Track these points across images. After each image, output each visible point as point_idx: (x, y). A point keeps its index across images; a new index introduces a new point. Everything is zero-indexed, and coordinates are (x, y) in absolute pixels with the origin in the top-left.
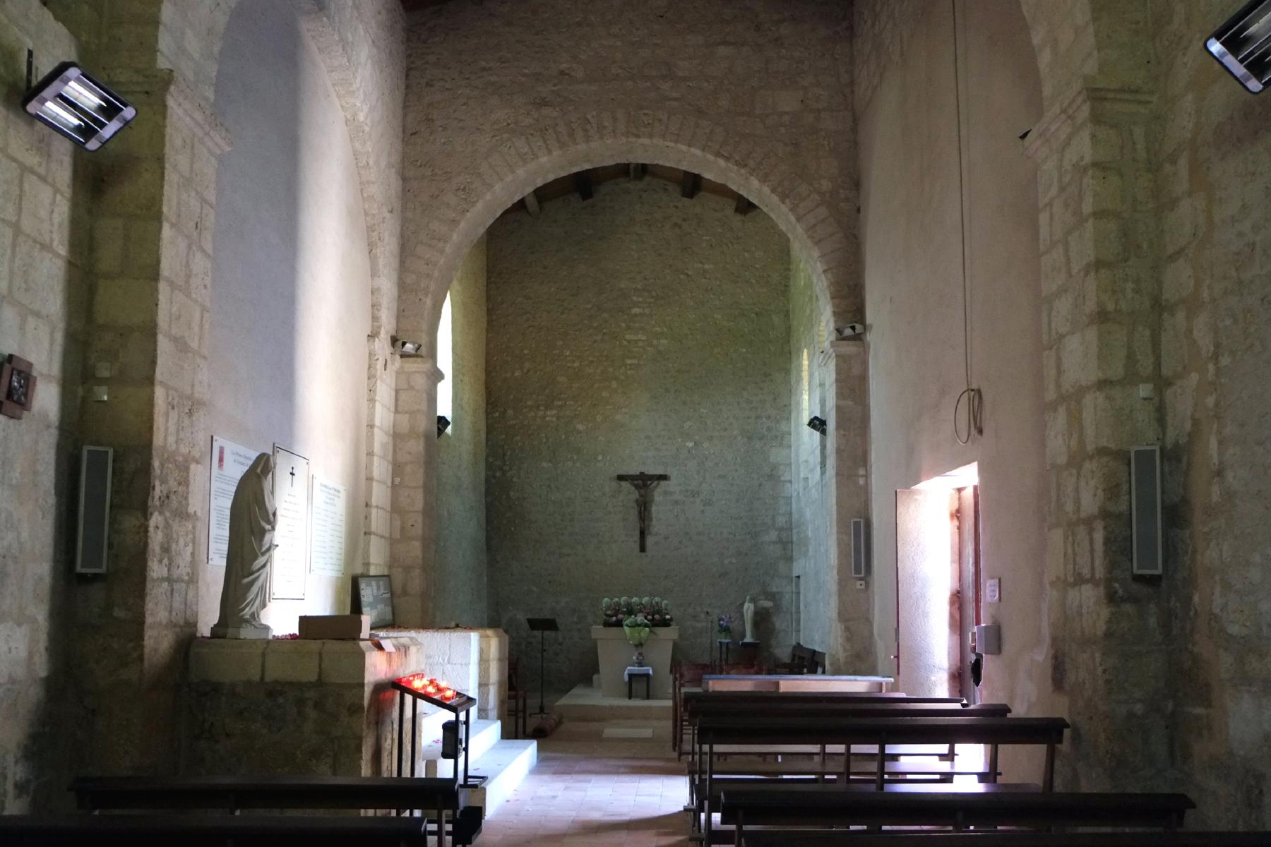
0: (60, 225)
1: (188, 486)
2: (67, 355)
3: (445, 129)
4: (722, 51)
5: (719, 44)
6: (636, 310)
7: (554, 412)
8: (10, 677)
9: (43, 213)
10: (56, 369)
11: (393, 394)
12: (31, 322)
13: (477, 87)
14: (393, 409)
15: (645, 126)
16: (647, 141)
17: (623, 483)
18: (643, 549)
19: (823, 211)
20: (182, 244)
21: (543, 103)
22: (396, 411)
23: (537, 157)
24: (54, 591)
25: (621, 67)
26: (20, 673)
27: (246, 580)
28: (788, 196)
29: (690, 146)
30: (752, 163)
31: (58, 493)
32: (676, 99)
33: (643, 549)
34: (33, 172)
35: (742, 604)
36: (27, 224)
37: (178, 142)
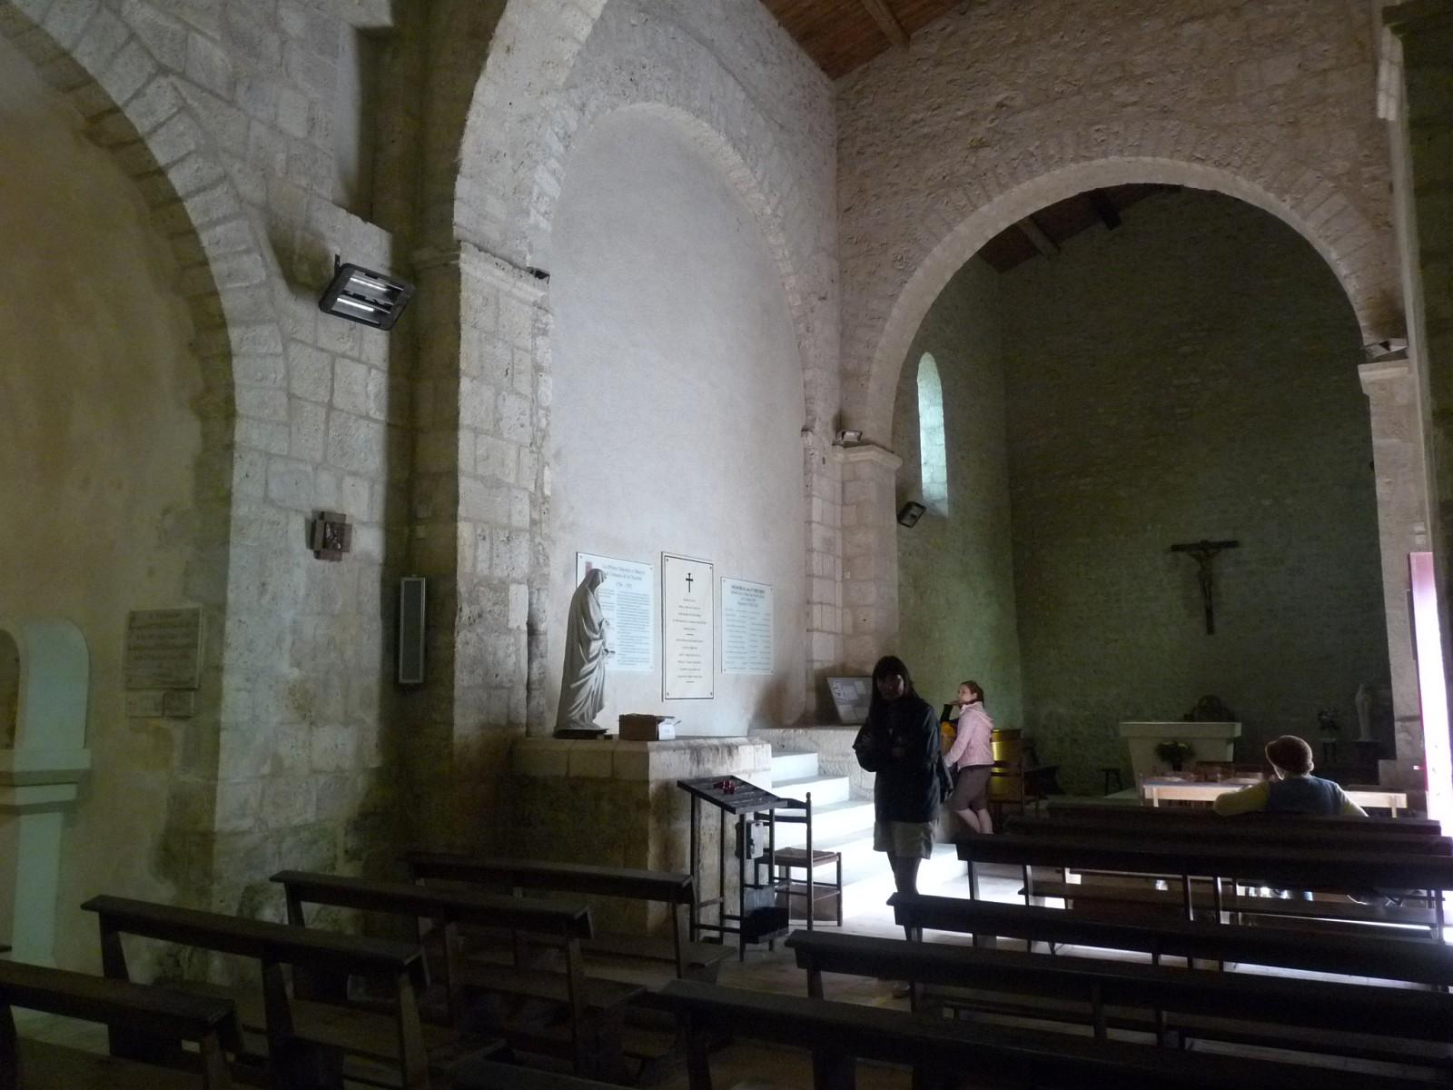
0: (376, 396)
1: (507, 605)
2: (389, 502)
3: (878, 196)
4: (1191, 29)
5: (1184, 22)
6: (1186, 349)
7: (1089, 479)
8: (338, 767)
9: (357, 388)
10: (378, 514)
11: (838, 486)
12: (349, 481)
13: (908, 145)
14: (839, 500)
15: (1098, 145)
16: (1102, 161)
17: (1181, 555)
18: (1210, 630)
19: (1340, 200)
20: (488, 393)
21: (981, 144)
22: (844, 504)
23: (976, 207)
24: (384, 697)
25: (1065, 82)
26: (347, 764)
27: (573, 686)
28: (1287, 191)
29: (1154, 156)
30: (1236, 161)
31: (384, 615)
32: (1135, 103)
33: (1210, 630)
34: (344, 356)
35: (1353, 696)
36: (339, 401)
37: (478, 302)
